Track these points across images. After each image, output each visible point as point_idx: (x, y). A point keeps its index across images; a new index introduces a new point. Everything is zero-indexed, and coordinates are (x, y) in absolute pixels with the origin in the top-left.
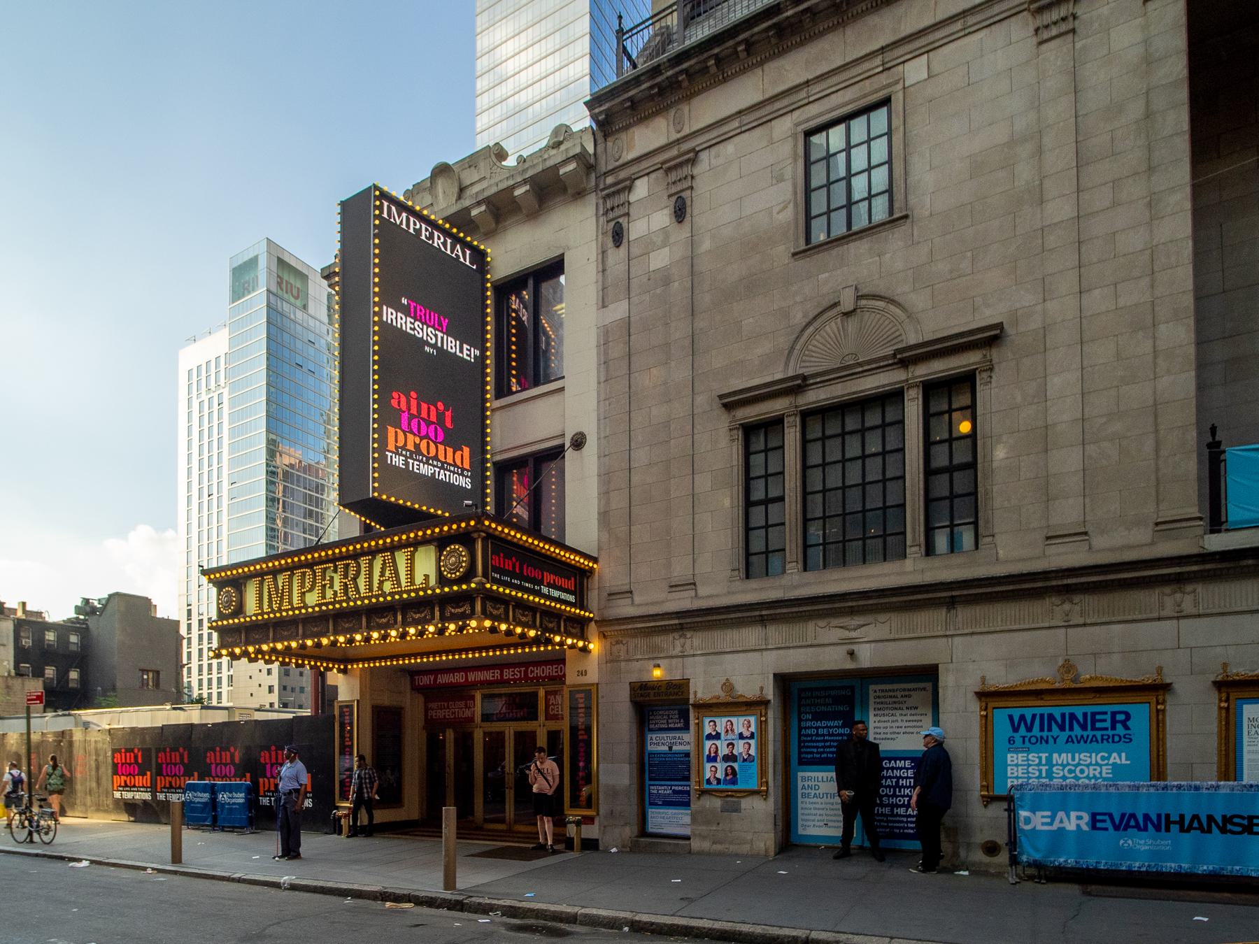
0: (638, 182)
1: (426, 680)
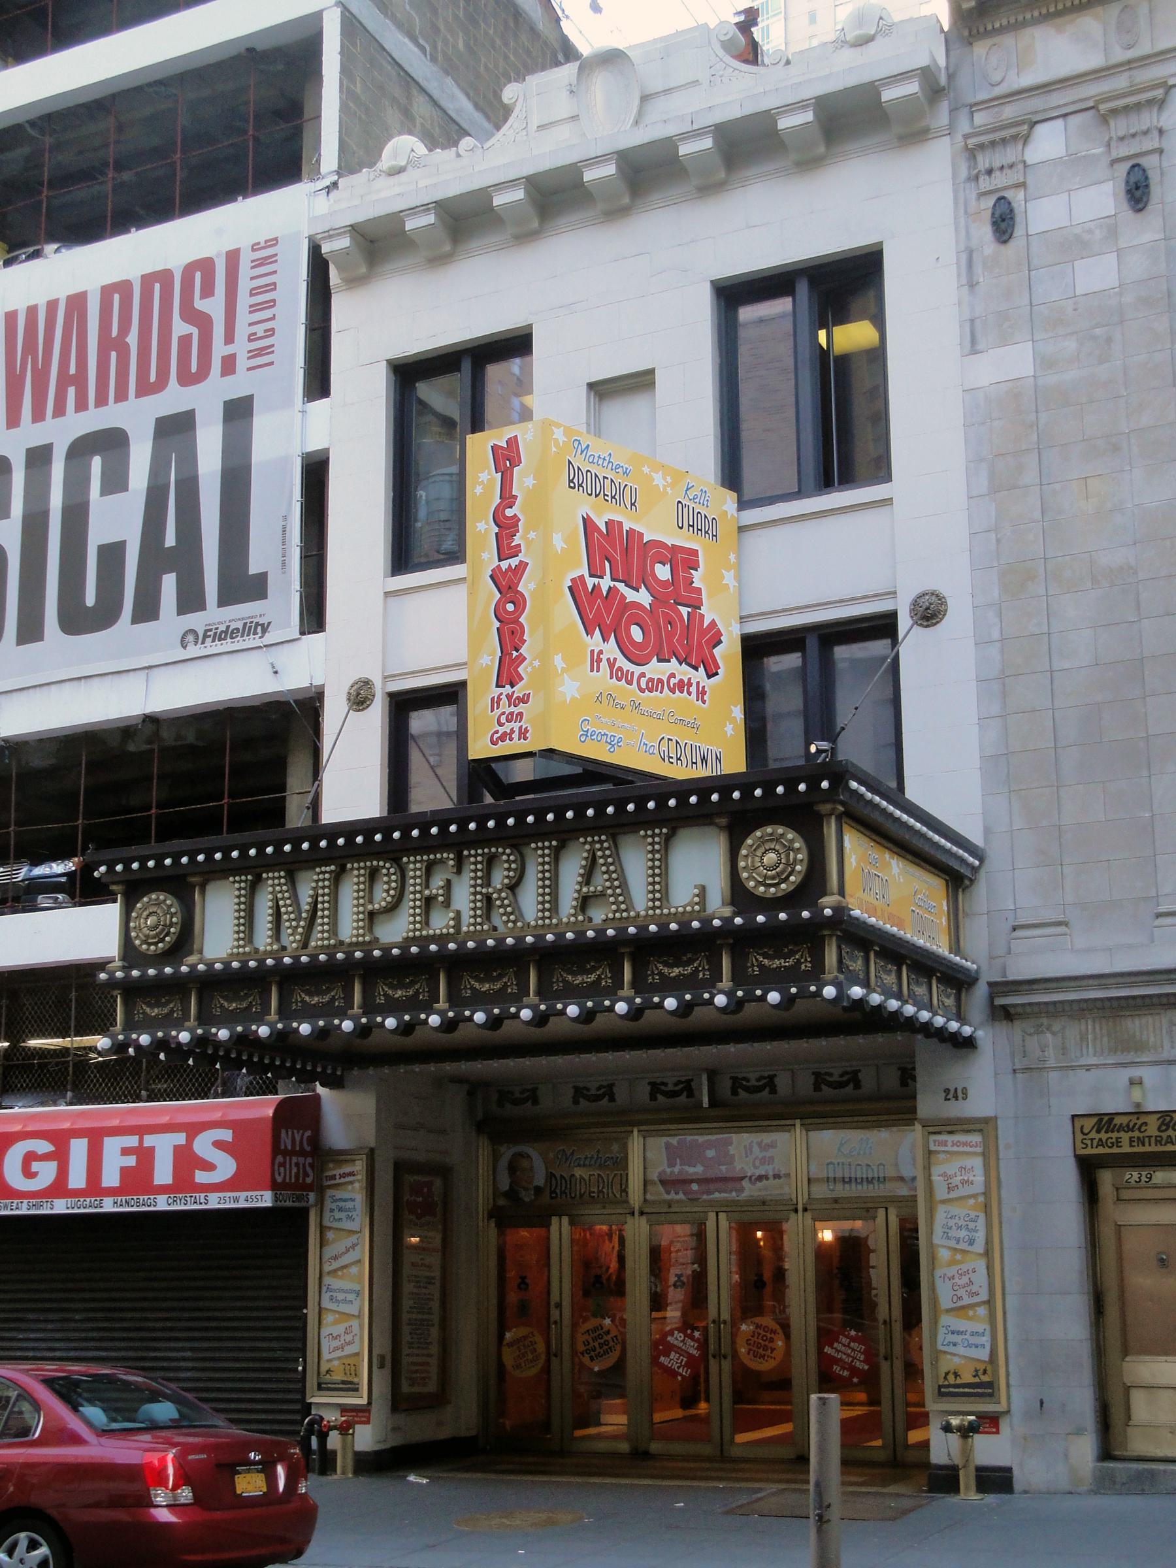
0: (1041, 130)
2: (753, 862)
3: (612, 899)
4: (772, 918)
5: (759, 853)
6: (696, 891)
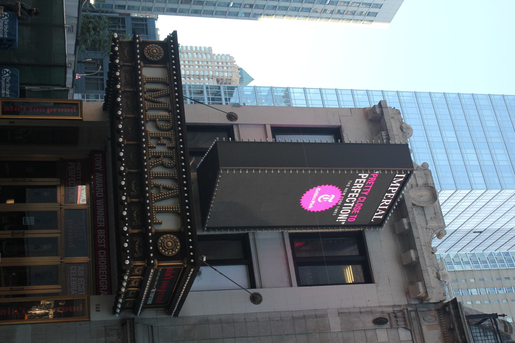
0: (409, 333)
1: (98, 164)
4: (151, 244)
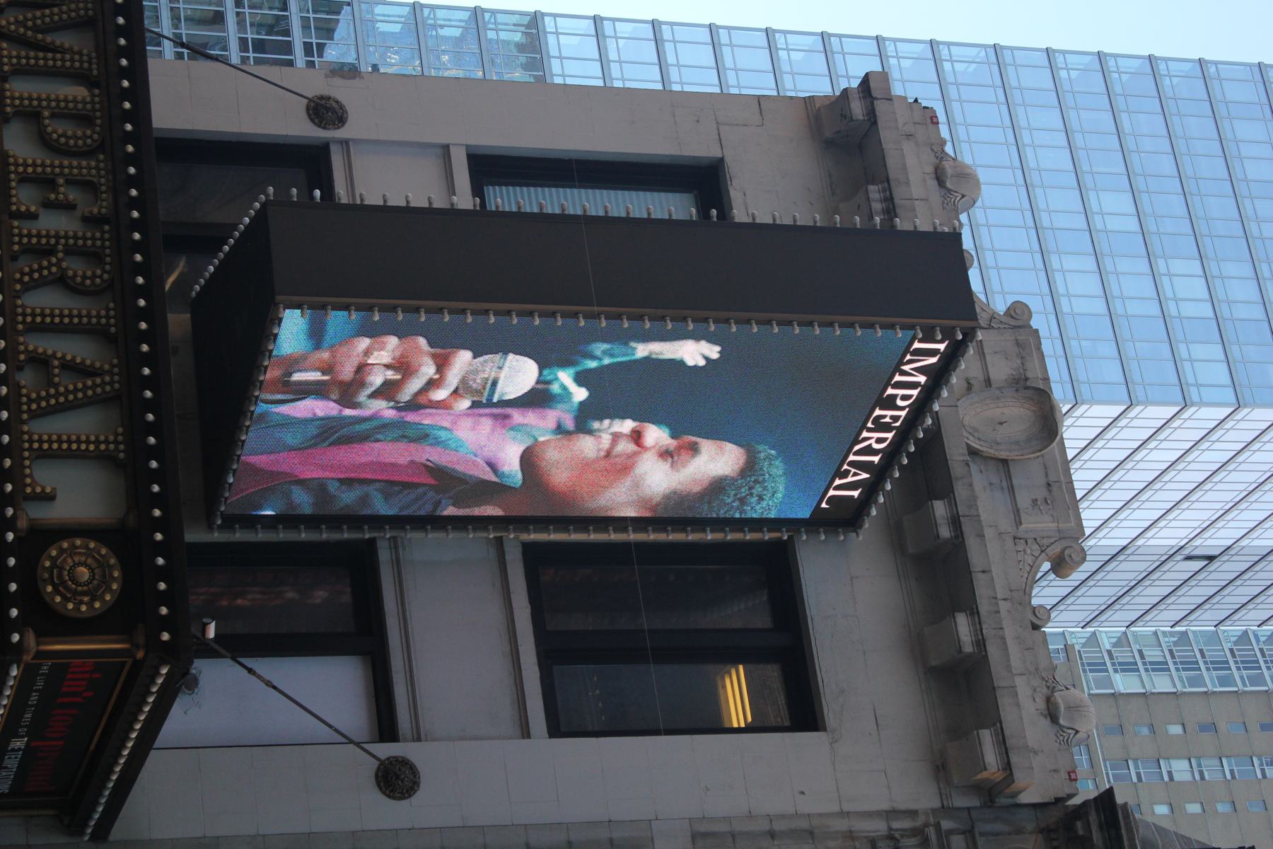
2: (80, 554)
3: (43, 393)
4: (11, 575)
5: (90, 561)
6: (48, 490)
